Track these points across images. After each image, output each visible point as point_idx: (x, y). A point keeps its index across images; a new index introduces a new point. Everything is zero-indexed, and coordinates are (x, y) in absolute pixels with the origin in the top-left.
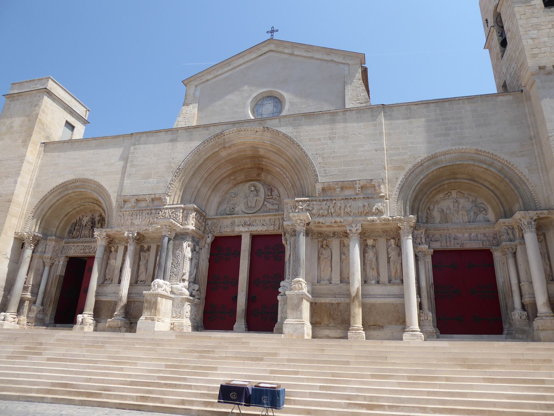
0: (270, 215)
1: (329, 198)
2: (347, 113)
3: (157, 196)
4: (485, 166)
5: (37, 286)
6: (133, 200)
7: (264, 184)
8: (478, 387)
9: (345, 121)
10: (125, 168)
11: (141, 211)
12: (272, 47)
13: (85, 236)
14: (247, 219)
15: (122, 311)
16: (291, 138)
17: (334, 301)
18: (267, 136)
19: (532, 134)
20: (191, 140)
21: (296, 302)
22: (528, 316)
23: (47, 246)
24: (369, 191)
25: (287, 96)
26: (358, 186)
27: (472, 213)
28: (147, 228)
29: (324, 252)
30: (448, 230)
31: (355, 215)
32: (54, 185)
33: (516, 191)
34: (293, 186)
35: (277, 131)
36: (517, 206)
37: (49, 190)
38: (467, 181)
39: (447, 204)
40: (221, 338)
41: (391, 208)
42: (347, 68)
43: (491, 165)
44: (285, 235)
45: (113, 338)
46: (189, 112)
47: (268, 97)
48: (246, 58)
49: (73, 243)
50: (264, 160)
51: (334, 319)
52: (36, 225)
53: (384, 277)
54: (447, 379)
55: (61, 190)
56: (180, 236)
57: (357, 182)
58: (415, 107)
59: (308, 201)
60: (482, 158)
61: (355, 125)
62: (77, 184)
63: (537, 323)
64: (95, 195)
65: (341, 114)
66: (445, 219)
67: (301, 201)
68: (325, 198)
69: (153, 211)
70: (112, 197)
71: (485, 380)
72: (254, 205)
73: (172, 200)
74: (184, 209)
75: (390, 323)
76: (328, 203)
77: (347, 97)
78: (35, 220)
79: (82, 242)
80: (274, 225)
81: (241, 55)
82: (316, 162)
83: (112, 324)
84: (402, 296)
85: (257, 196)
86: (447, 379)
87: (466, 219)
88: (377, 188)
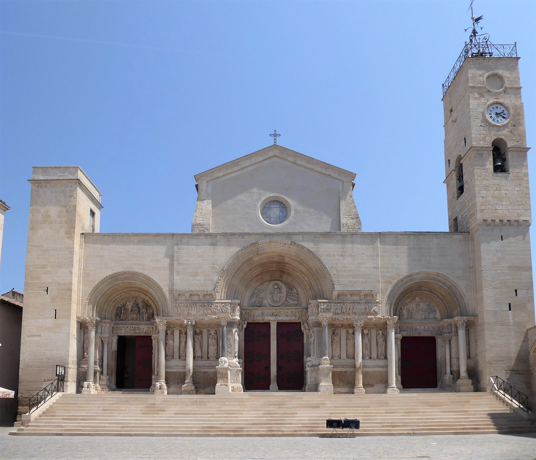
0: (292, 309)
1: (342, 302)
2: (354, 236)
3: (209, 293)
4: (441, 284)
5: (102, 359)
6: (187, 295)
7: (285, 284)
8: (439, 415)
9: (352, 242)
10: (171, 265)
11: (194, 303)
12: (277, 152)
13: (133, 319)
14: (274, 311)
15: (191, 379)
16: (313, 253)
17: (343, 370)
18: (293, 249)
19: (471, 265)
20: (229, 245)
21: (326, 372)
22: (454, 378)
23: (103, 328)
24: (369, 298)
25: (292, 203)
26: (362, 294)
27: (427, 313)
28: (203, 317)
29: (335, 337)
30: (412, 324)
31: (359, 314)
32: (104, 276)
33: (457, 303)
34: (310, 289)
35: (303, 246)
36: (455, 312)
37: (100, 280)
38: (428, 292)
39: (412, 306)
40: (281, 396)
41: (382, 311)
42: (341, 184)
43: (444, 284)
44: (303, 324)
45: (204, 399)
46: (204, 208)
47: (275, 201)
48: (254, 160)
49: (122, 325)
50: (287, 265)
51: (343, 381)
52: (93, 311)
53: (374, 355)
54: (423, 412)
55: (111, 280)
56: (231, 324)
57: (362, 292)
58: (401, 237)
59: (327, 302)
60: (440, 278)
61: (359, 246)
62: (126, 276)
63: (459, 382)
64: (145, 287)
65: (349, 236)
66: (411, 316)
67: (322, 302)
68: (339, 301)
69: (206, 304)
70: (164, 290)
71: (441, 412)
72: (278, 300)
73: (220, 297)
74: (231, 304)
75: (377, 383)
76: (342, 305)
77: (341, 212)
78: (91, 306)
79: (132, 324)
81: (249, 157)
82: (333, 273)
83: (187, 388)
84: (387, 366)
86: (423, 412)
87: (423, 317)
88: (374, 296)
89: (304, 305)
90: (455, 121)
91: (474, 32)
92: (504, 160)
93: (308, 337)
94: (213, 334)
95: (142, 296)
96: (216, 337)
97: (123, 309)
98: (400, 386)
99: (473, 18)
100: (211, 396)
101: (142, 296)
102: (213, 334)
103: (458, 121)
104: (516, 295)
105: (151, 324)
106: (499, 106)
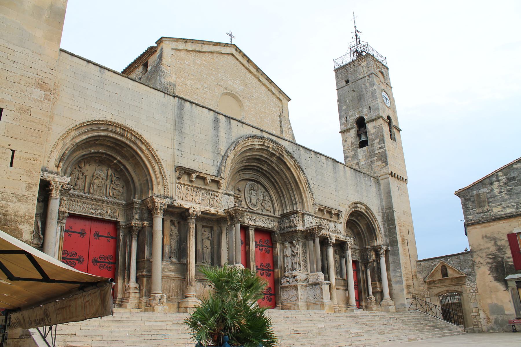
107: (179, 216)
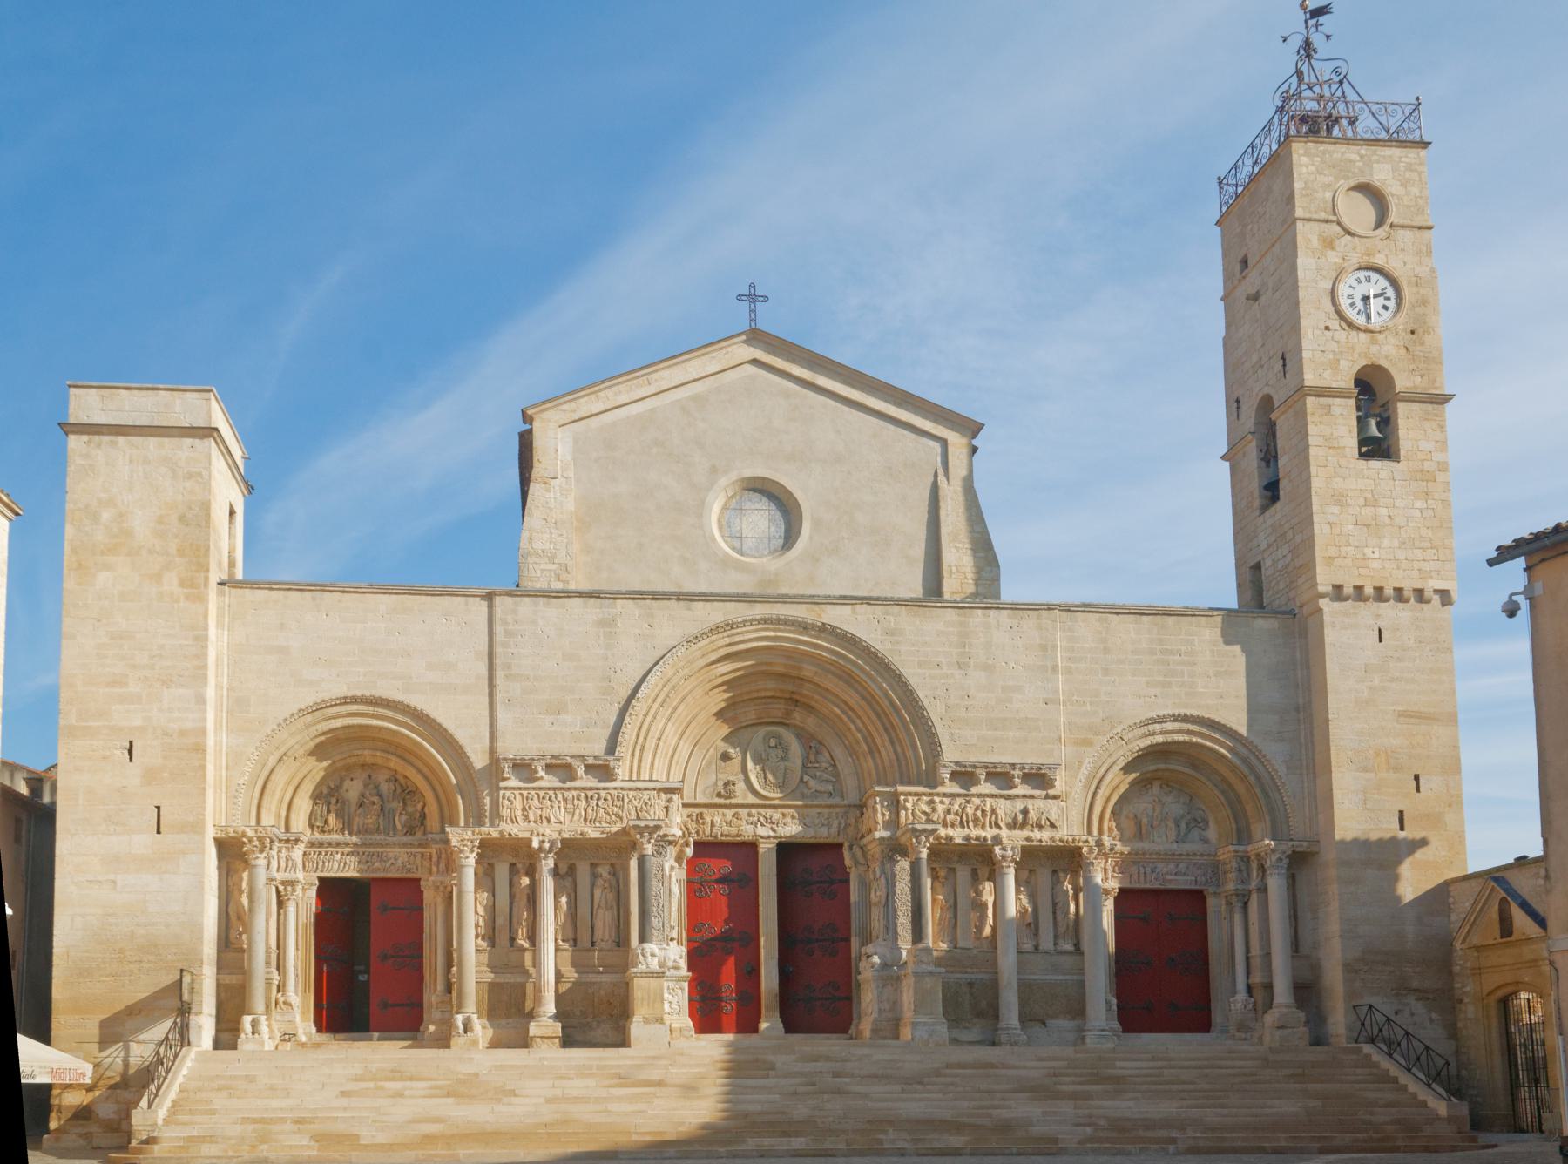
7: (801, 734)
19: (1301, 701)
27: (1183, 826)
44: (851, 848)
80: (829, 826)
85: (784, 759)
89: (852, 797)
90: (1255, 297)
91: (1308, 48)
92: (1386, 422)
93: (865, 886)
94: (605, 874)
95: (394, 763)
96: (614, 882)
97: (333, 800)
98: (1116, 1025)
99: (1303, 7)
100: (622, 1050)
101: (394, 763)
102: (605, 874)
103: (1263, 299)
104: (1418, 790)
105: (420, 846)
106: (1374, 276)
107: (509, 860)
